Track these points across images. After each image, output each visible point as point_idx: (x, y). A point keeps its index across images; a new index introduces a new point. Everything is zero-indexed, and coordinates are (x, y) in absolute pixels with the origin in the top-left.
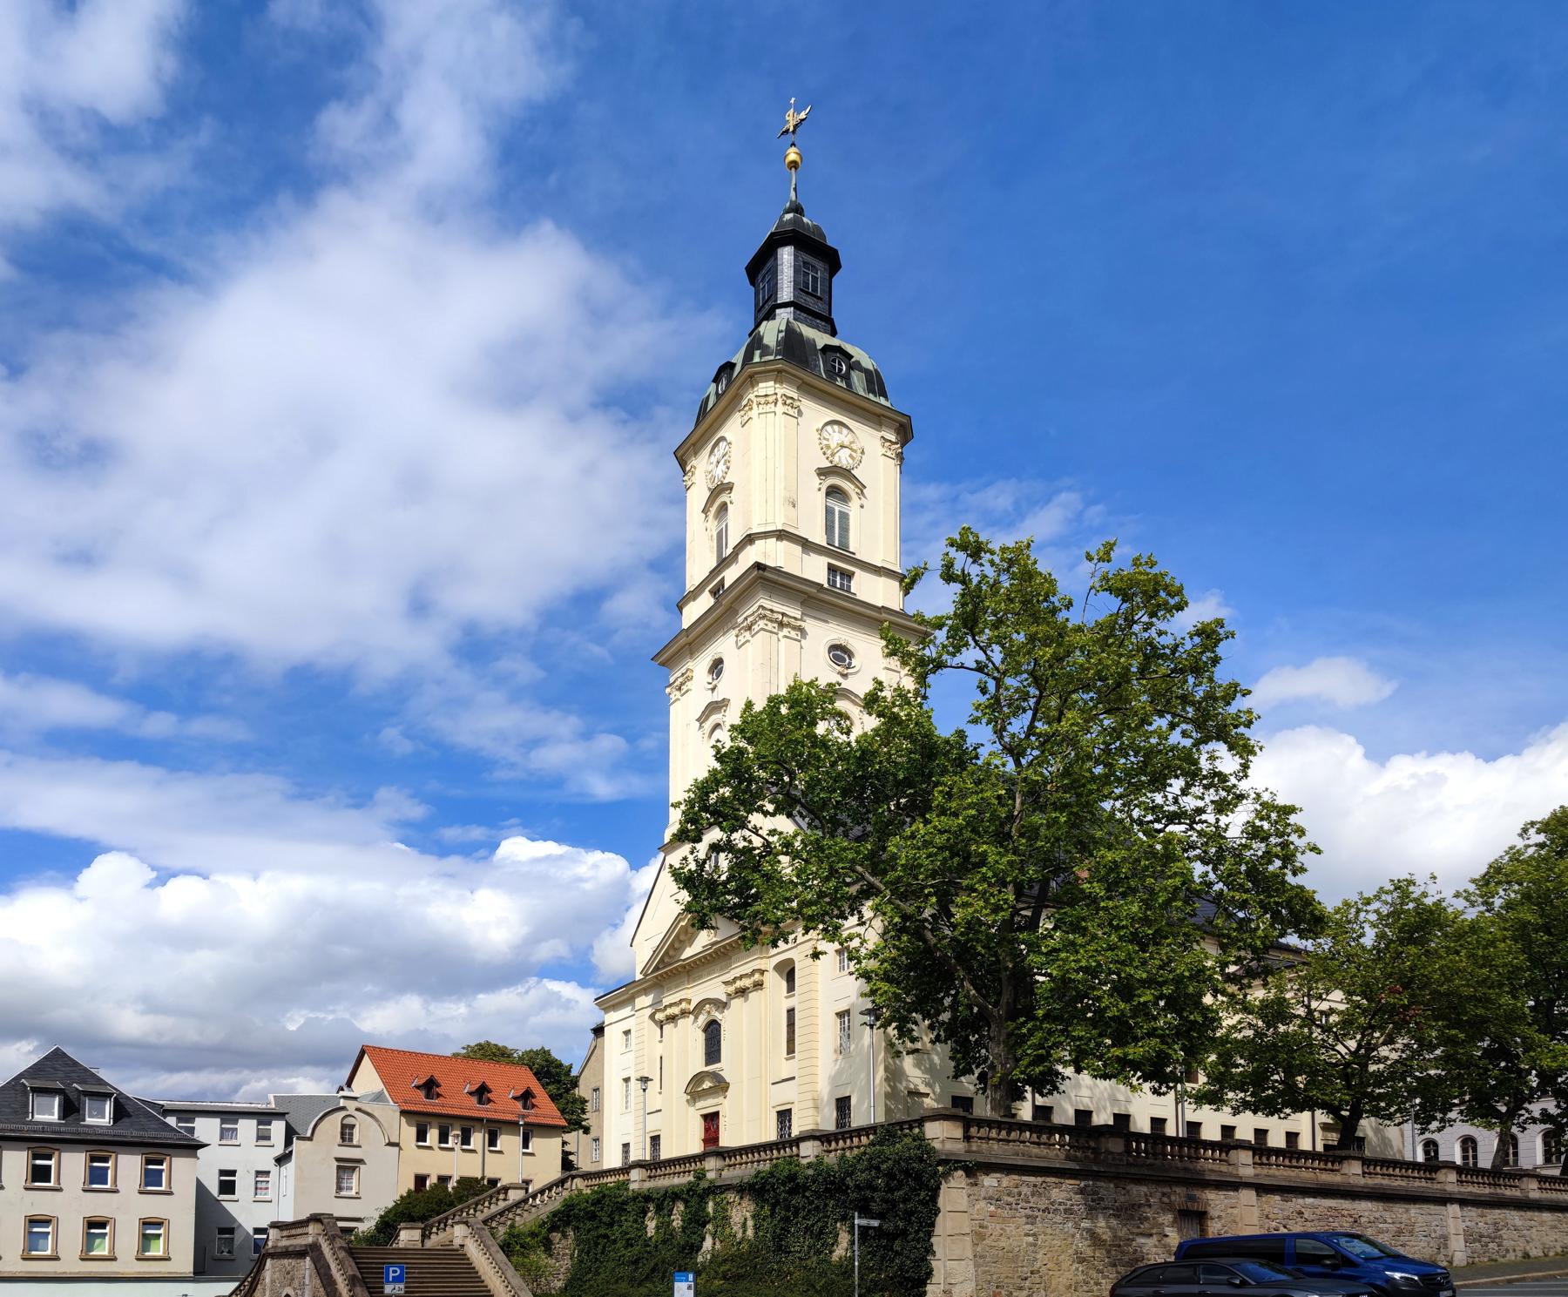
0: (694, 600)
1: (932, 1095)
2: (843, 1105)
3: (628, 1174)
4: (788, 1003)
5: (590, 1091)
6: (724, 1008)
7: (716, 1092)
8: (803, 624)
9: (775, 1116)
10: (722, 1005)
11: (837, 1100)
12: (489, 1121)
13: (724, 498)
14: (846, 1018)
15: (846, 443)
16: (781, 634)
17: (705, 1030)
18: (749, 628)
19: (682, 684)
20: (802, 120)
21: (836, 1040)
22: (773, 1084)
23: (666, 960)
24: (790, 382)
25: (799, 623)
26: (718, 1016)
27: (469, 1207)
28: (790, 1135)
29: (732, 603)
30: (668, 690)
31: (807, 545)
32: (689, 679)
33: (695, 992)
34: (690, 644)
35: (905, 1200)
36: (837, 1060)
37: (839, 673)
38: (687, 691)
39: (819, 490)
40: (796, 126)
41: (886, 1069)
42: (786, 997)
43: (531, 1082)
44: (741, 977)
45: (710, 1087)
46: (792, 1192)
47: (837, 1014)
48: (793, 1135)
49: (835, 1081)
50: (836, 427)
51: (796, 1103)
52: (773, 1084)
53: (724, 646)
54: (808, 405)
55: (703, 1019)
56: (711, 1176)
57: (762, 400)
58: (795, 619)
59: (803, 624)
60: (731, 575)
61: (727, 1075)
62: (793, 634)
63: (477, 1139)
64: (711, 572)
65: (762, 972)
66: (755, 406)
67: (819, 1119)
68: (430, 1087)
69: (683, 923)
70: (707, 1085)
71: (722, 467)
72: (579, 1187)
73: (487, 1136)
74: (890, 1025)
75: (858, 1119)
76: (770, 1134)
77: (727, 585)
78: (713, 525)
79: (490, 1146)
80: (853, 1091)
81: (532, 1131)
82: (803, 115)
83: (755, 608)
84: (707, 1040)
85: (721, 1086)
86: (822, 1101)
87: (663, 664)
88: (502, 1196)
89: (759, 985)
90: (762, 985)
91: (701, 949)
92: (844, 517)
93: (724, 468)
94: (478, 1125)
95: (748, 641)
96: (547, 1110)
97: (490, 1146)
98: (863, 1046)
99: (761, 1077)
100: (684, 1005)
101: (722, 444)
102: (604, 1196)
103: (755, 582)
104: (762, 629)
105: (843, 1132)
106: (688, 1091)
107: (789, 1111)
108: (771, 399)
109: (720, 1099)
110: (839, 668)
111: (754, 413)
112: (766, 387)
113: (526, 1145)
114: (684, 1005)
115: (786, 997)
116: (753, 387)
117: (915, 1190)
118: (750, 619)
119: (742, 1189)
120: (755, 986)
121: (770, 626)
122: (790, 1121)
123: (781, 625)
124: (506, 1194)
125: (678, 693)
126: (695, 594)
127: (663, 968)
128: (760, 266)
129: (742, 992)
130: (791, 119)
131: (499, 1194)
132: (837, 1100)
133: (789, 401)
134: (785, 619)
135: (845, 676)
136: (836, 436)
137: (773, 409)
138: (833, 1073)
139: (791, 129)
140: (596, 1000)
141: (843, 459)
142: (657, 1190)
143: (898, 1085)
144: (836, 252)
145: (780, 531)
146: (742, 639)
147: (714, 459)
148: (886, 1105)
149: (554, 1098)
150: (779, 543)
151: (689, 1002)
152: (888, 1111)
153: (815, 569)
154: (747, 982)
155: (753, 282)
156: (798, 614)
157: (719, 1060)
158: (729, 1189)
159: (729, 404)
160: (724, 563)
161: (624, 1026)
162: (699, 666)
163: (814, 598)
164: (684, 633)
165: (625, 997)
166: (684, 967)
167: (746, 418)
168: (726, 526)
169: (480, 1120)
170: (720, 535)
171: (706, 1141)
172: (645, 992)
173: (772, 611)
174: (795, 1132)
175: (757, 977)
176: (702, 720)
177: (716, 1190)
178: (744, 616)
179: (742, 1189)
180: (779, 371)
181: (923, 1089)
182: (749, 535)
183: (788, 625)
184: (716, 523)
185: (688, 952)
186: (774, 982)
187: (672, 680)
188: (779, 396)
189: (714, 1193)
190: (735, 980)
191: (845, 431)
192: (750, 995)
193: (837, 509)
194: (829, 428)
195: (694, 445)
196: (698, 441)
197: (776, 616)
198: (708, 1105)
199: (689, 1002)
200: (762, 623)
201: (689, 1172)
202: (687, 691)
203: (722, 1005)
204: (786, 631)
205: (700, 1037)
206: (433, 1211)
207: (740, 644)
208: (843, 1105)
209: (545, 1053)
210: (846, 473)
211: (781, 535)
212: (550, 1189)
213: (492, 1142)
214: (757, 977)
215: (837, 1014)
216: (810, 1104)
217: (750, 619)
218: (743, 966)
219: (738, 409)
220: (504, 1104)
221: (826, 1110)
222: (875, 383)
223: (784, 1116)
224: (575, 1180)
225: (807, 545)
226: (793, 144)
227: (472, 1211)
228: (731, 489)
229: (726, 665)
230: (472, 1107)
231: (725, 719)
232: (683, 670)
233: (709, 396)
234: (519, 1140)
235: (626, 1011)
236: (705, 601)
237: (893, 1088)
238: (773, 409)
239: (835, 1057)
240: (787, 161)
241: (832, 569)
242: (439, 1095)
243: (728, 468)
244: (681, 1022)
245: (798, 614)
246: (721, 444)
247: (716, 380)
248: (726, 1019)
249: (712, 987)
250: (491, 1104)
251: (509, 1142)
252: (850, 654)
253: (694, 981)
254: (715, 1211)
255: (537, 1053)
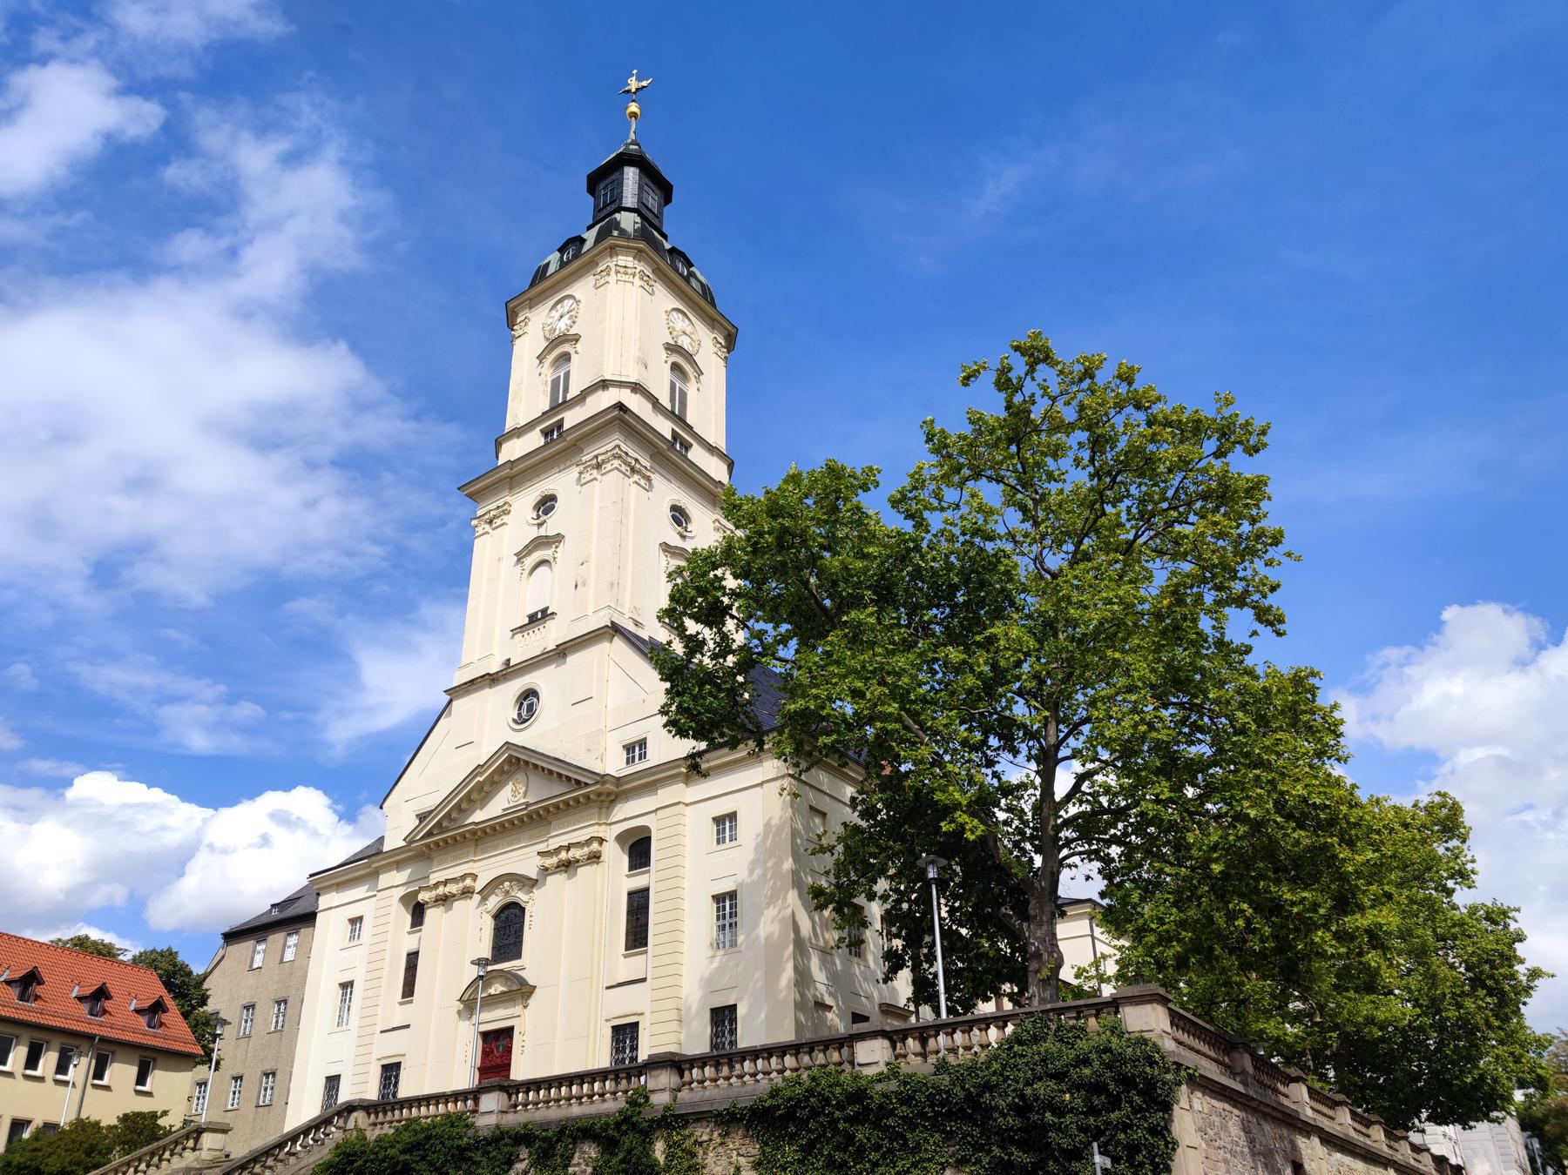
0: (518, 437)
1: (835, 1008)
2: (723, 1017)
3: (1117, 1012)
4: (410, 943)
5: (237, 1006)
6: (533, 886)
7: (512, 1000)
8: (652, 476)
9: (608, 1033)
10: (529, 883)
11: (712, 1010)
12: (103, 1040)
13: (566, 348)
14: (349, 990)
15: (688, 332)
16: (632, 480)
17: (496, 917)
18: (598, 466)
19: (495, 517)
20: (644, 87)
21: (712, 929)
22: (608, 988)
23: (445, 824)
24: (648, 263)
25: (648, 474)
26: (521, 896)
27: (140, 1160)
28: (394, 1095)
29: (578, 441)
30: (474, 522)
31: (655, 403)
32: (507, 512)
33: (487, 867)
34: (512, 478)
35: (1125, 1127)
36: (713, 957)
37: (679, 533)
38: (502, 525)
39: (666, 362)
40: (637, 89)
41: (796, 968)
42: (409, 933)
43: (159, 991)
44: (446, 883)
45: (503, 993)
46: (854, 1120)
47: (340, 984)
48: (640, 1060)
49: (710, 986)
50: (680, 315)
51: (647, 1014)
52: (608, 988)
53: (561, 482)
54: (659, 289)
55: (495, 902)
56: (660, 1099)
57: (622, 270)
58: (646, 468)
59: (652, 476)
60: (571, 418)
61: (530, 976)
62: (642, 482)
63: (81, 1068)
64: (544, 414)
65: (601, 841)
66: (613, 273)
67: (682, 1036)
68: (28, 983)
69: (480, 779)
70: (496, 989)
71: (566, 321)
72: (361, 1125)
73: (94, 1062)
74: (826, 907)
75: (747, 1037)
76: (602, 1058)
77: (567, 426)
78: (548, 372)
79: (94, 1078)
80: (741, 999)
81: (154, 1060)
82: (645, 83)
83: (612, 445)
84: (497, 930)
85: (521, 991)
86: (689, 1009)
87: (470, 496)
88: (191, 1143)
89: (595, 858)
90: (599, 857)
91: (500, 813)
92: (683, 395)
93: (569, 322)
94: (84, 1046)
95: (595, 479)
96: (176, 1030)
97: (94, 1078)
98: (758, 937)
99: (591, 978)
100: (468, 882)
101: (568, 303)
102: (428, 1138)
103: (614, 421)
104: (617, 468)
105: (387, 1103)
106: (465, 998)
107: (635, 1026)
108: (629, 271)
109: (518, 1010)
110: (679, 528)
111: (612, 278)
112: (625, 260)
113: (141, 1080)
114: (468, 882)
115: (628, 876)
116: (611, 257)
117: (1141, 1110)
118: (492, 513)
119: (728, 1119)
120: (589, 858)
121: (623, 468)
122: (397, 1077)
123: (633, 470)
124: (197, 1140)
125: (487, 526)
126: (519, 432)
127: (437, 834)
128: (602, 179)
129: (568, 866)
130: (633, 84)
131: (188, 1139)
132: (712, 1010)
133: (645, 278)
134: (637, 466)
135: (683, 537)
136: (680, 323)
137: (631, 279)
138: (707, 973)
139: (633, 90)
140: (311, 876)
141: (685, 342)
142: (545, 1126)
143: (806, 991)
144: (671, 187)
145: (636, 384)
146: (587, 477)
147: (555, 314)
148: (797, 1020)
149: (186, 1015)
150: (633, 395)
151: (474, 877)
152: (799, 1027)
153: (665, 427)
154: (453, 888)
155: (592, 190)
156: (648, 465)
157: (518, 955)
158: (698, 1120)
159: (581, 268)
160: (557, 407)
161: (353, 912)
162: (523, 502)
163: (662, 455)
164: (509, 464)
165: (367, 871)
166: (474, 833)
167: (602, 281)
168: (567, 375)
169: (89, 1037)
170: (555, 383)
171: (484, 1071)
172: (398, 865)
173: (627, 454)
174: (643, 1055)
175: (595, 846)
176: (521, 556)
177: (672, 1121)
178: (595, 453)
179: (728, 1119)
180: (640, 251)
181: (829, 1001)
182: (604, 381)
183: (639, 472)
184: (551, 371)
185: (479, 816)
186: (613, 856)
187: (480, 513)
188: (637, 271)
189: (669, 1126)
190: (557, 851)
191: (686, 321)
192: (455, 904)
193: (678, 385)
194: (675, 313)
195: (531, 300)
196: (535, 297)
197: (629, 460)
198: (494, 1019)
199: (474, 877)
200: (616, 463)
201: (382, 1124)
202: (502, 525)
203: (529, 883)
204: (636, 477)
205: (488, 925)
206: (78, 1164)
207: (583, 481)
208: (723, 1017)
209: (170, 955)
210: (689, 357)
211: (636, 388)
212: (317, 1128)
213: (99, 1074)
214: (595, 846)
215: (340, 984)
216: (674, 1015)
217: (492, 513)
218: (563, 836)
219: (593, 272)
220: (123, 1019)
221: (695, 1024)
222: (706, 293)
223: (625, 1034)
224: (354, 1115)
225: (655, 403)
226: (633, 101)
227: (143, 1166)
228: (577, 341)
229: (559, 506)
230: (79, 1018)
231: (556, 555)
232: (500, 503)
233: (548, 264)
234: (133, 1071)
235: (360, 891)
236: (535, 440)
237: (802, 995)
238: (631, 279)
239: (710, 953)
240: (628, 111)
241: (675, 434)
242: (37, 998)
243: (574, 322)
244: (458, 905)
245: (648, 465)
246: (566, 302)
247: (562, 250)
248: (537, 906)
249: (523, 858)
250: (107, 1016)
251: (121, 1073)
252: (688, 519)
253: (483, 853)
254: (670, 1157)
255: (162, 954)
